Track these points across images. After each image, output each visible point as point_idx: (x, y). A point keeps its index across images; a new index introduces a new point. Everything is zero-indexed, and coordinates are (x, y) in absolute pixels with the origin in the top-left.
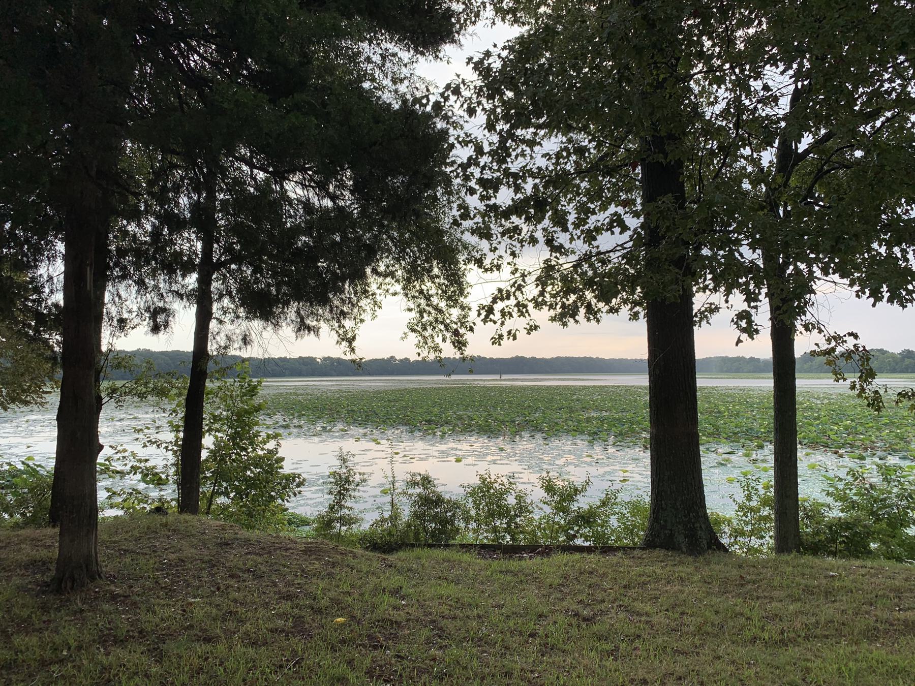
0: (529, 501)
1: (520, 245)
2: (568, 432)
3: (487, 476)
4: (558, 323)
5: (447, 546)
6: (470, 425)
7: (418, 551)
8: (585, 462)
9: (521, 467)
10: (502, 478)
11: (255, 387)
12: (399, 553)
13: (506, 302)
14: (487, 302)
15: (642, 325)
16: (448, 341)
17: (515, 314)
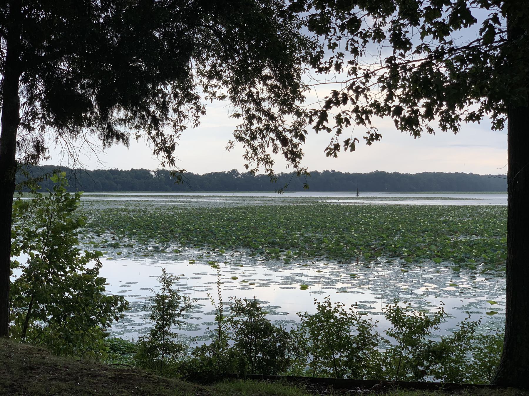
0: (373, 333)
1: (362, 40)
2: (431, 258)
3: (326, 304)
4: (409, 132)
5: (274, 378)
6: (319, 249)
7: (241, 383)
8: (449, 292)
9: (374, 296)
10: (343, 307)
11: (73, 201)
12: (218, 385)
13: (342, 107)
14: (320, 107)
15: (503, 135)
16: (280, 152)
17: (353, 121)
